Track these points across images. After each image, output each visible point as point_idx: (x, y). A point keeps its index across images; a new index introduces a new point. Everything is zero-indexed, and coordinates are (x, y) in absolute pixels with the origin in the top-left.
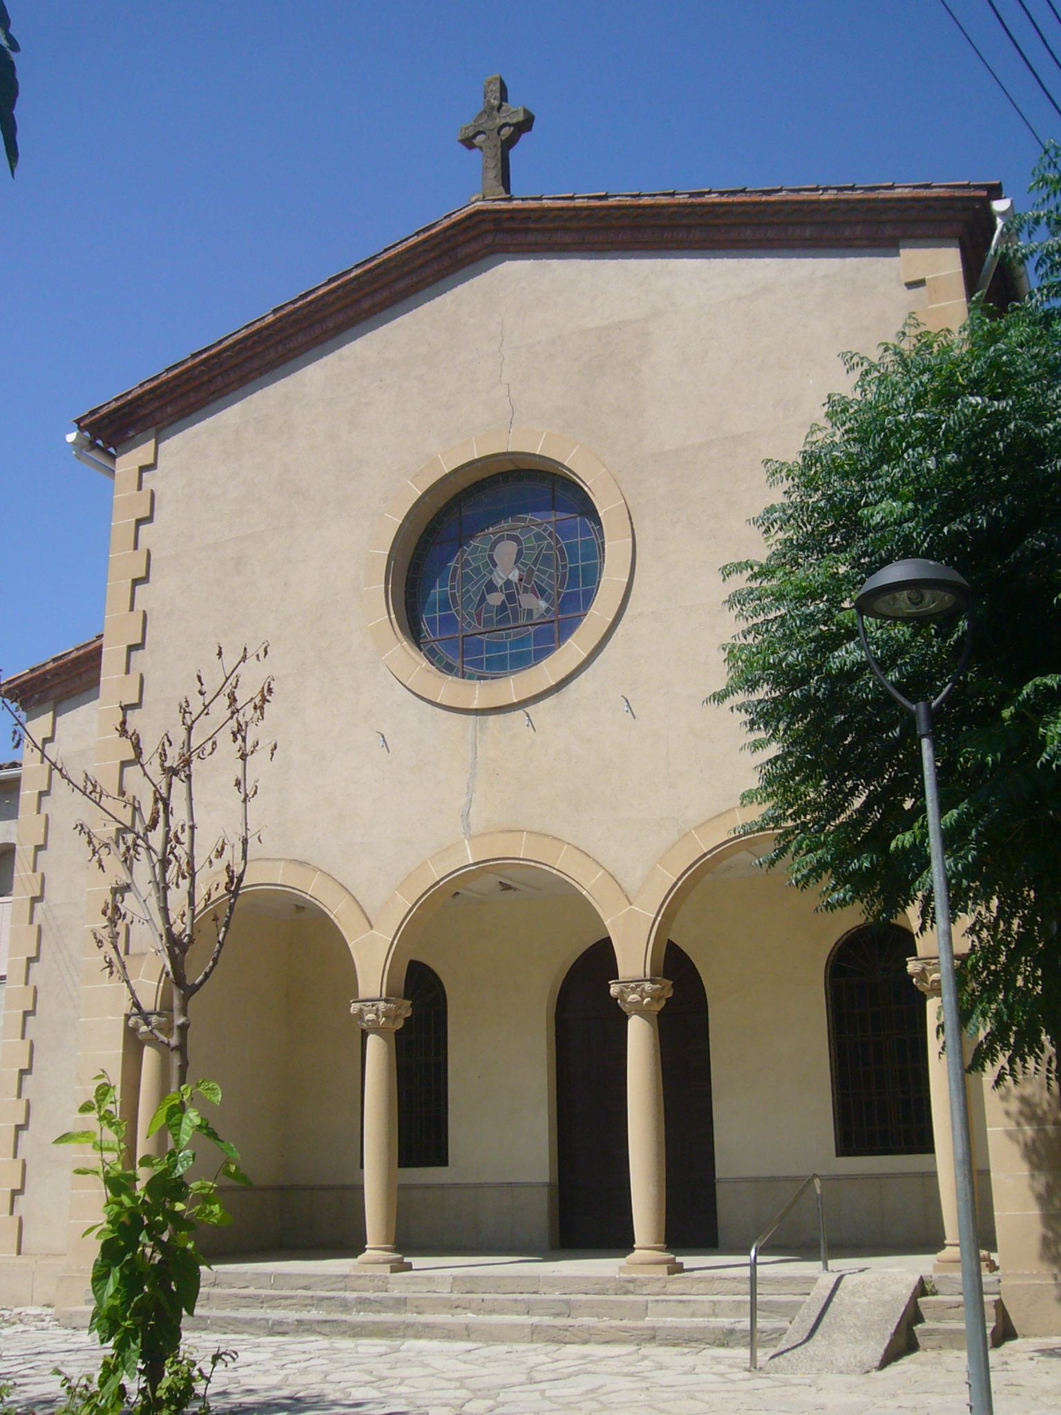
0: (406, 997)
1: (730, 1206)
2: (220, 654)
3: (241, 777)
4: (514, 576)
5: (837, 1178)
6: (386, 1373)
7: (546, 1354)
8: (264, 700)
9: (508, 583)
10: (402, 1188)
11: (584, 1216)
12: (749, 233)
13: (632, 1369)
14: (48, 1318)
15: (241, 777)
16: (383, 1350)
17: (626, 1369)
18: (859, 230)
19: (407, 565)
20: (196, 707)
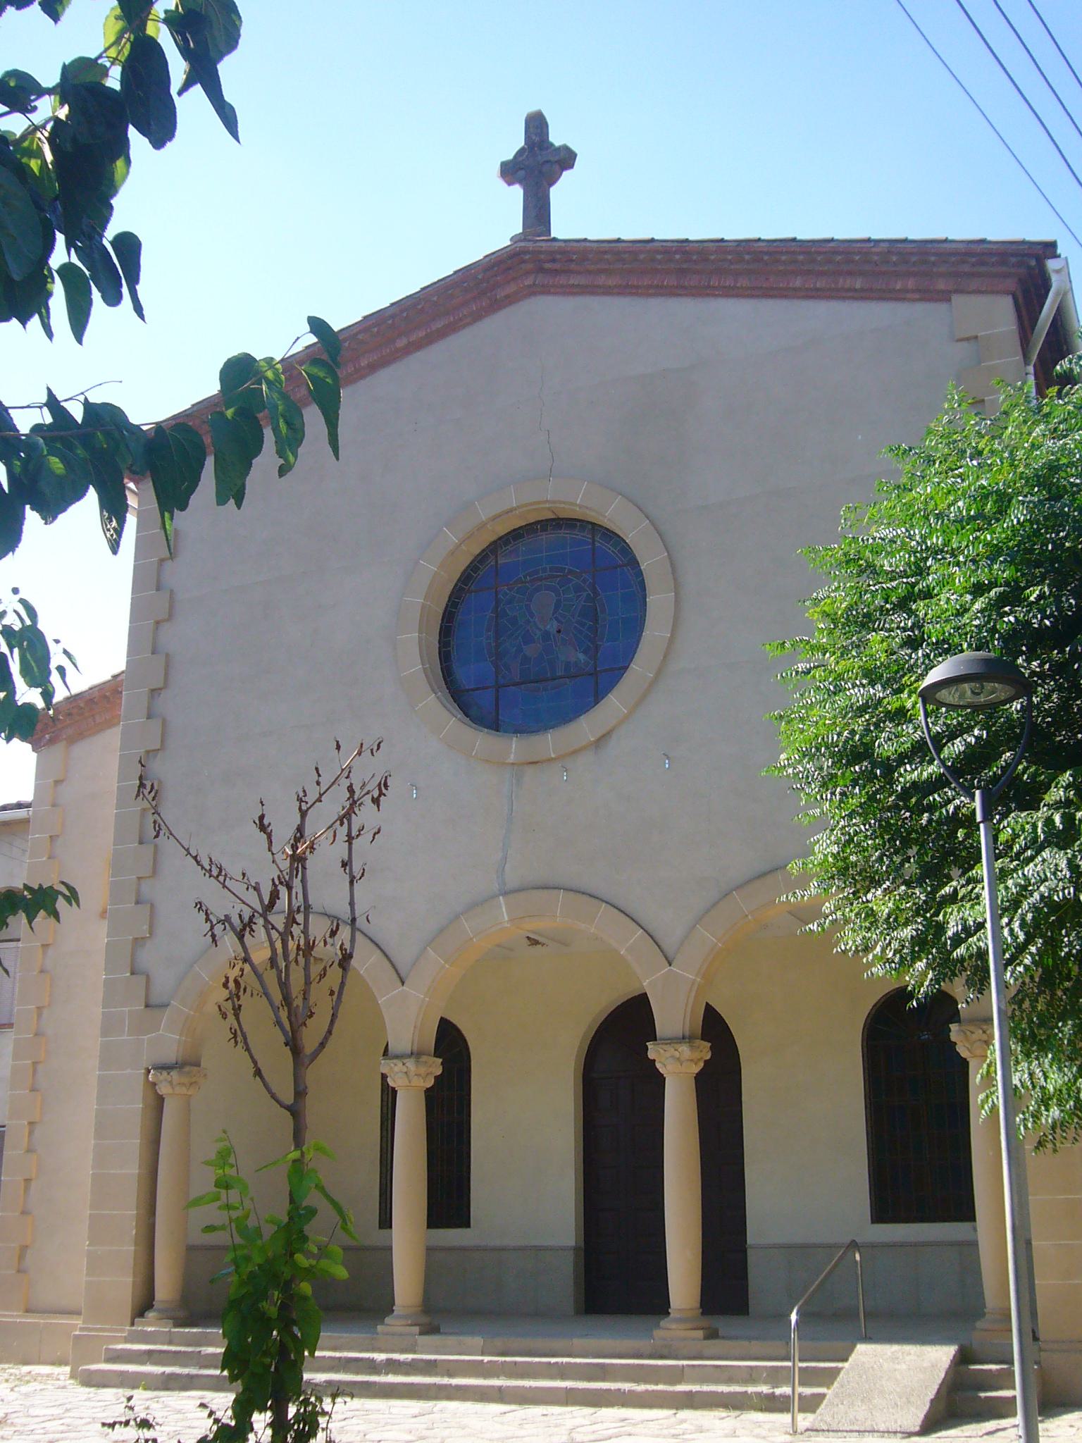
0: (436, 1055)
1: (762, 1275)
2: (338, 747)
3: (346, 858)
4: (552, 627)
5: (873, 1246)
6: (425, 1433)
7: (584, 1417)
8: (381, 794)
9: (546, 636)
10: (430, 1250)
11: (612, 1280)
12: (798, 282)
13: (673, 1431)
14: (62, 1377)
15: (346, 858)
16: (416, 1411)
17: (665, 1432)
18: (911, 283)
19: (441, 612)
20: (311, 798)
